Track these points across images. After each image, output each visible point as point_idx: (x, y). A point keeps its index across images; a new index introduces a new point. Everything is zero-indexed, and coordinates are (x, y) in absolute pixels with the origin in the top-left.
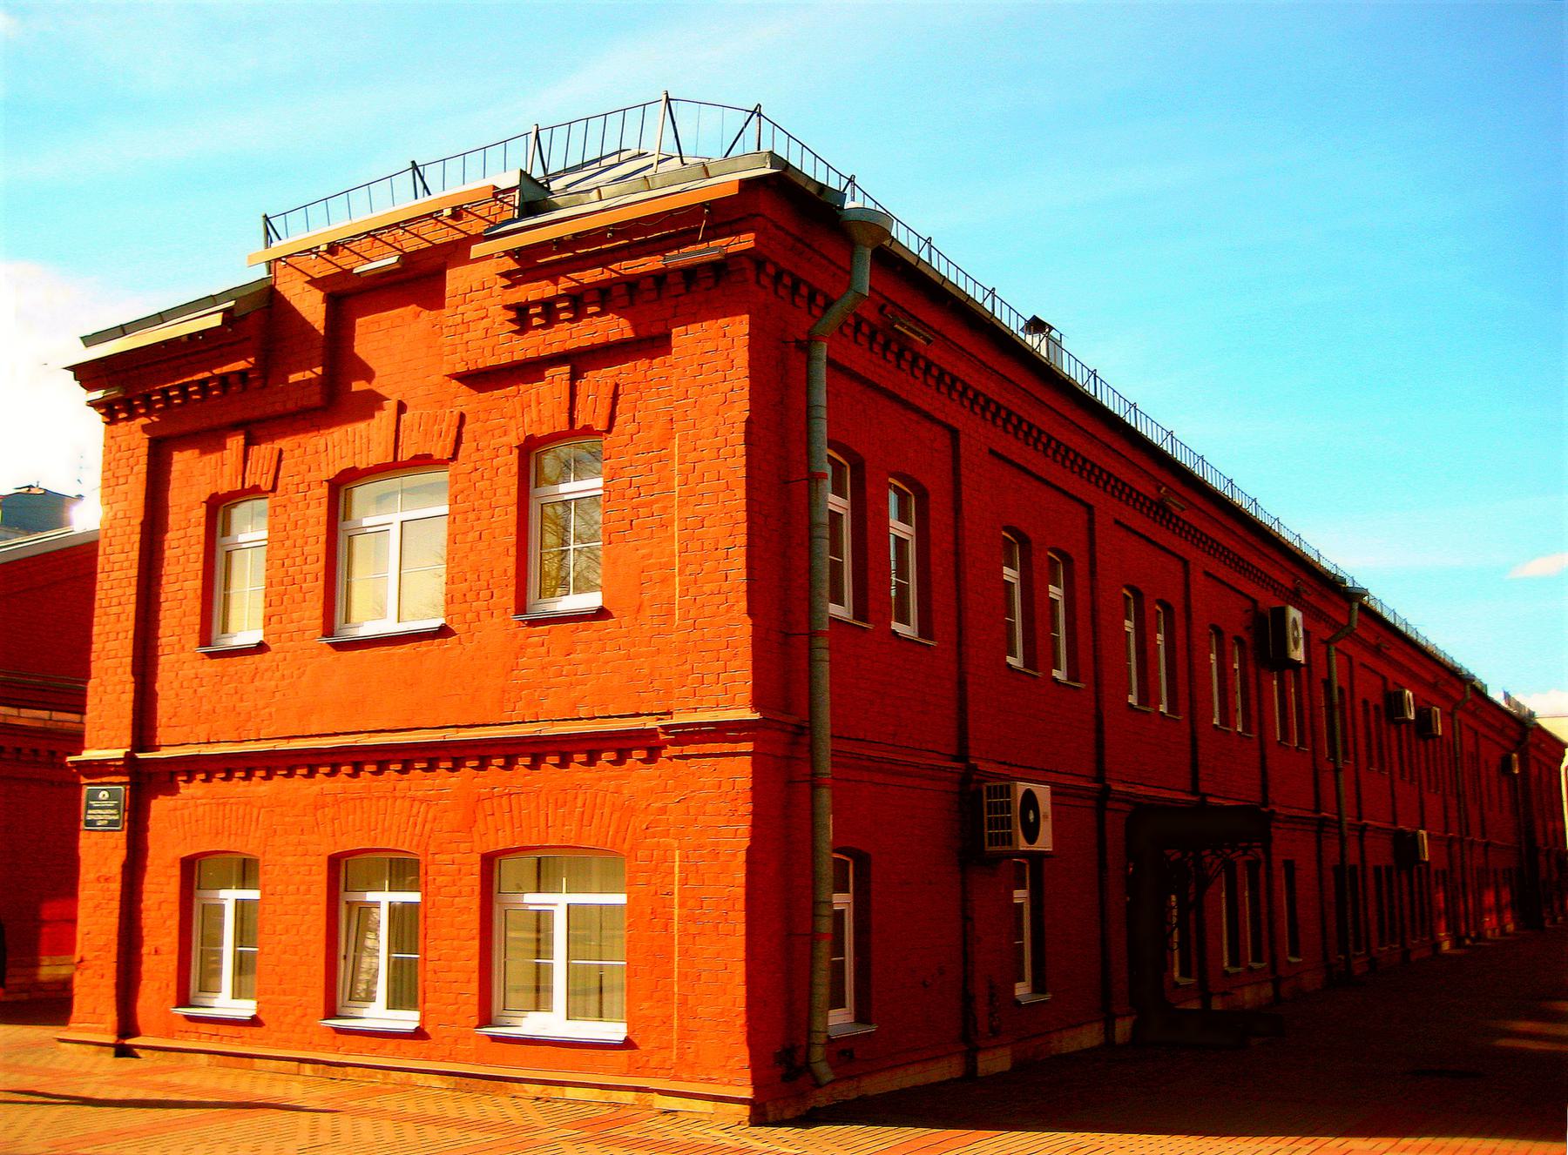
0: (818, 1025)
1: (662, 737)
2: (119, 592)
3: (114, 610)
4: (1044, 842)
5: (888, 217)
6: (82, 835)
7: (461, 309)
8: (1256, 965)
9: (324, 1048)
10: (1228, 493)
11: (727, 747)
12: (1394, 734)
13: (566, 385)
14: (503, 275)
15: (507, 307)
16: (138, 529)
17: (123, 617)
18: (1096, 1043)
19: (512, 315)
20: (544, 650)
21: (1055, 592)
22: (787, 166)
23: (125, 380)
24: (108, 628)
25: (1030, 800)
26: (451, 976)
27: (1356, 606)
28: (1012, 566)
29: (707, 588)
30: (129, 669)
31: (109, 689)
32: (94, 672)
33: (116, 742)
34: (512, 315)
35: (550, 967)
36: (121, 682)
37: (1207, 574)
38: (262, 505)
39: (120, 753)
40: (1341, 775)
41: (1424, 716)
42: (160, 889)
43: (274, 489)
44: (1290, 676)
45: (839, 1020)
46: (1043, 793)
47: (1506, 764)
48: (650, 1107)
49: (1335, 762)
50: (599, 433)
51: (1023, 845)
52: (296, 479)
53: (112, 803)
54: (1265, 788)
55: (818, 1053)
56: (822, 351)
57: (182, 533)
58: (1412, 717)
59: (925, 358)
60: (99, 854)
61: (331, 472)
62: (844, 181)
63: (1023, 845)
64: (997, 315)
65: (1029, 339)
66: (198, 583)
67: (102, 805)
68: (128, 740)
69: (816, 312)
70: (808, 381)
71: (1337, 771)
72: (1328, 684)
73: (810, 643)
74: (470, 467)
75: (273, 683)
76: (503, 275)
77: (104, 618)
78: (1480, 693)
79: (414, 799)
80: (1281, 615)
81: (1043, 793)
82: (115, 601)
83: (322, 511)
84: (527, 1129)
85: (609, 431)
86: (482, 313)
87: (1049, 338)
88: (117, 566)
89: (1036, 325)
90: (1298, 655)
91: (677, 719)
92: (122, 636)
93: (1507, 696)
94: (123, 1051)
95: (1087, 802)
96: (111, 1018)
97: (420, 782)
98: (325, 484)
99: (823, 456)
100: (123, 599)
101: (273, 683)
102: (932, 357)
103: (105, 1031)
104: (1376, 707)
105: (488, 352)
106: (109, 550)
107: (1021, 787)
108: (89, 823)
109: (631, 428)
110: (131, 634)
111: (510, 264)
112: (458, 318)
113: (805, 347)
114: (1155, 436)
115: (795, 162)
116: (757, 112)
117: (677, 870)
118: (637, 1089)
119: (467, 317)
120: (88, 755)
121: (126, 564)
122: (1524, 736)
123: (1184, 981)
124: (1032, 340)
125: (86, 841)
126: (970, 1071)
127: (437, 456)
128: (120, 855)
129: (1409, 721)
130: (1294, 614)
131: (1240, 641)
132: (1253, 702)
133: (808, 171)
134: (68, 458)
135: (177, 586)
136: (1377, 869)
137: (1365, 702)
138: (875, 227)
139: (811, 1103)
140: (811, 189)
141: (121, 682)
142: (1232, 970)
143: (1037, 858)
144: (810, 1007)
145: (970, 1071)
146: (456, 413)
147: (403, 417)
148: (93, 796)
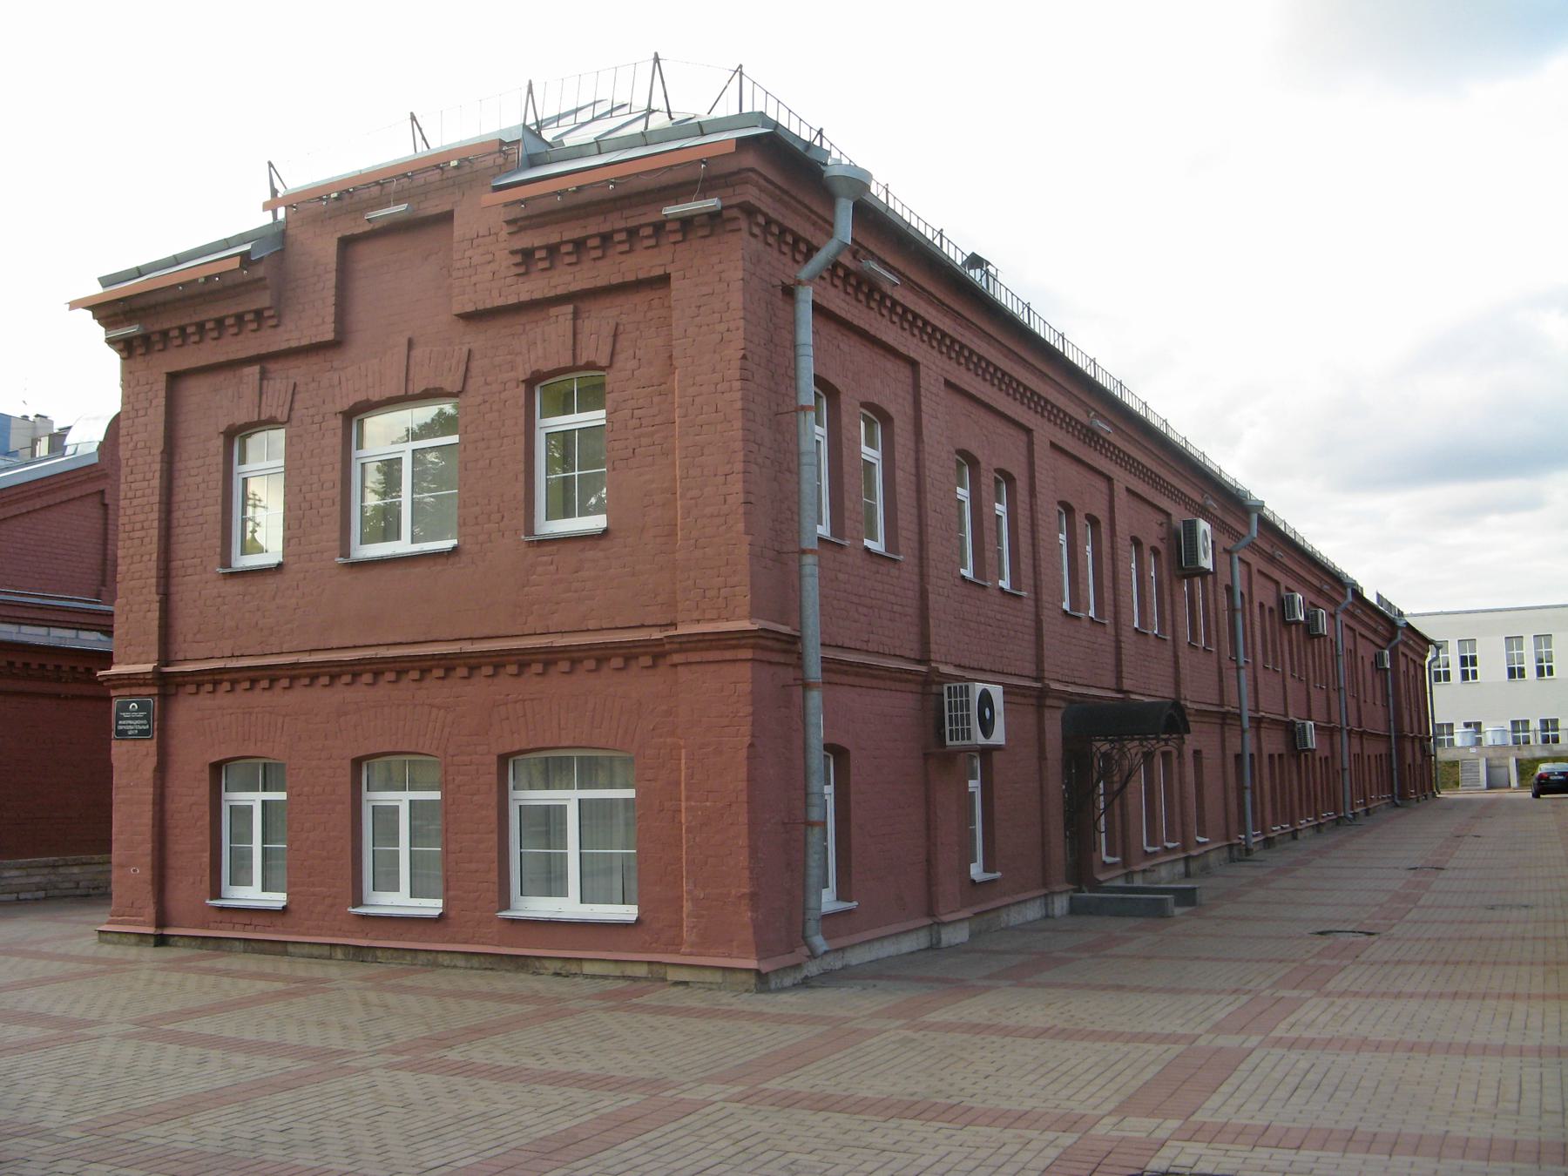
0: (812, 903)
1: (667, 647)
2: (142, 517)
3: (138, 534)
4: (998, 737)
5: (869, 176)
6: (114, 743)
7: (468, 254)
8: (1170, 845)
9: (352, 934)
10: (1142, 413)
11: (729, 655)
12: (1286, 637)
13: (569, 324)
14: (508, 222)
15: (513, 253)
16: (158, 458)
17: (147, 540)
18: (1038, 916)
19: (518, 259)
20: (552, 568)
21: (1001, 509)
22: (777, 125)
23: (147, 317)
24: (131, 551)
25: (986, 699)
26: (473, 866)
27: (1255, 517)
28: (962, 486)
29: (708, 510)
30: (154, 589)
31: (135, 608)
32: (119, 593)
33: (143, 657)
34: (518, 259)
35: (564, 858)
36: (146, 601)
37: (1128, 490)
38: (278, 436)
39: (149, 667)
40: (1243, 672)
41: (1312, 619)
42: (189, 792)
43: (289, 420)
44: (1198, 581)
45: (828, 900)
46: (996, 692)
47: (1378, 659)
48: (664, 980)
49: (1236, 661)
50: (602, 369)
51: (979, 739)
52: (312, 411)
53: (141, 714)
54: (1177, 684)
55: (812, 926)
56: (806, 296)
57: (200, 462)
58: (1302, 618)
59: (891, 298)
60: (130, 763)
61: (346, 404)
62: (814, 133)
63: (979, 739)
64: (945, 250)
65: (972, 273)
66: (218, 508)
67: (130, 714)
68: (155, 656)
69: (799, 257)
70: (793, 324)
71: (1238, 668)
72: (1230, 590)
73: (800, 560)
74: (479, 399)
75: (294, 601)
76: (508, 222)
77: (128, 543)
78: (1358, 594)
79: (432, 706)
80: (1191, 527)
81: (996, 692)
82: (138, 526)
83: (338, 440)
84: (558, 1000)
85: (610, 366)
86: (490, 257)
87: (987, 272)
88: (139, 493)
89: (976, 261)
90: (1207, 563)
91: (683, 630)
92: (146, 558)
93: (1379, 596)
94: (161, 941)
95: (1031, 698)
96: (150, 912)
97: (435, 690)
98: (340, 417)
99: (807, 392)
100: (146, 525)
101: (294, 601)
102: (897, 296)
103: (143, 924)
104: (1271, 610)
105: (495, 293)
106: (130, 478)
107: (979, 687)
108: (119, 733)
109: (633, 364)
110: (155, 556)
111: (518, 212)
112: (467, 262)
113: (789, 292)
114: (1081, 362)
115: (783, 122)
116: (739, 70)
117: (683, 766)
118: (650, 963)
119: (474, 261)
120: (115, 670)
121: (148, 491)
122: (1393, 635)
123: (1109, 860)
124: (975, 274)
125: (118, 749)
126: (934, 947)
127: (449, 389)
128: (152, 762)
129: (1298, 623)
130: (1204, 526)
131: (1155, 551)
132: (1167, 607)
133: (794, 129)
134: (79, 393)
135: (197, 512)
136: (1271, 756)
137: (1261, 605)
138: (858, 183)
139: (805, 972)
140: (800, 147)
141: (146, 601)
142: (1150, 849)
143: (986, 752)
144: (805, 887)
145: (934, 947)
146: (465, 349)
147: (415, 353)
148: (124, 707)
